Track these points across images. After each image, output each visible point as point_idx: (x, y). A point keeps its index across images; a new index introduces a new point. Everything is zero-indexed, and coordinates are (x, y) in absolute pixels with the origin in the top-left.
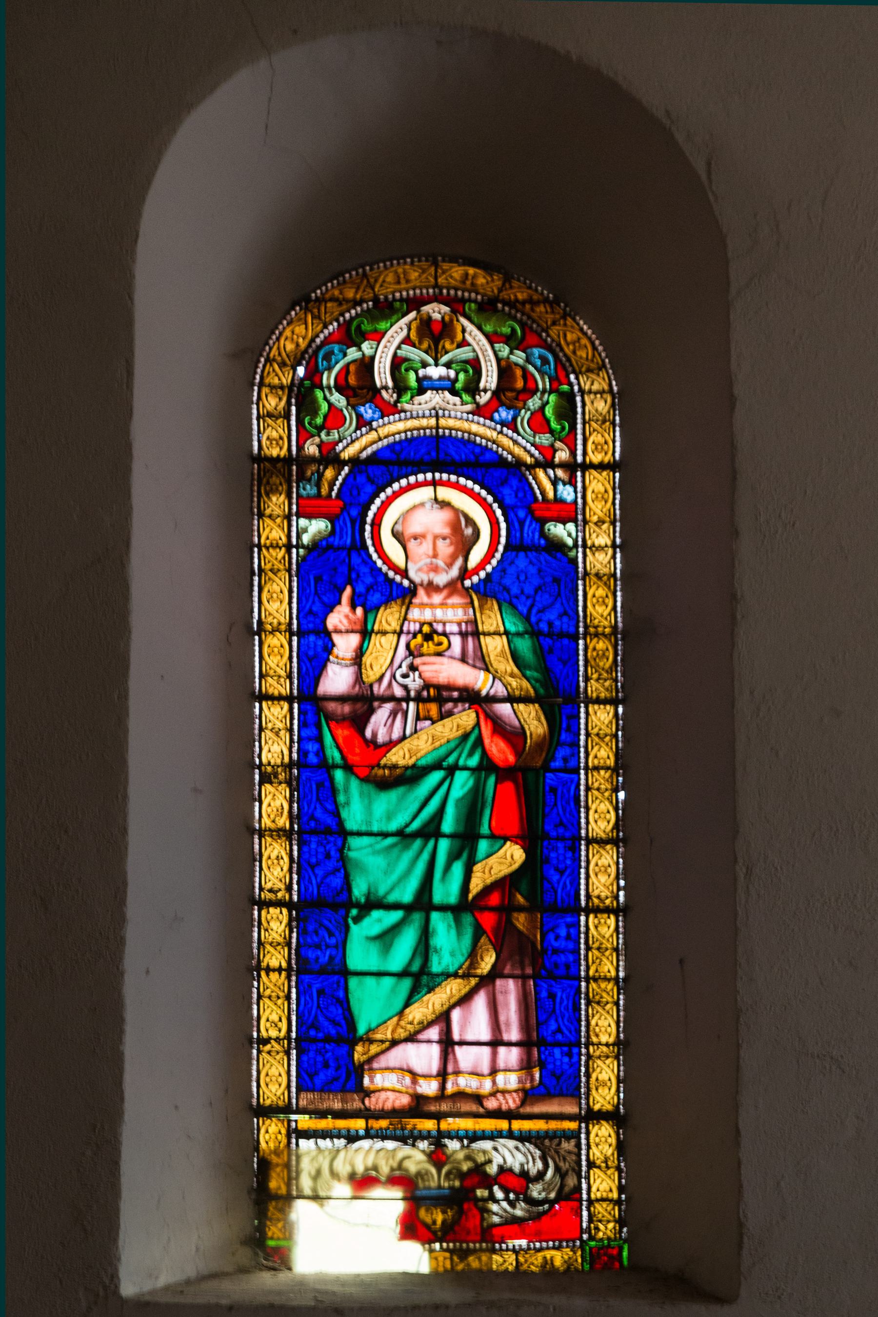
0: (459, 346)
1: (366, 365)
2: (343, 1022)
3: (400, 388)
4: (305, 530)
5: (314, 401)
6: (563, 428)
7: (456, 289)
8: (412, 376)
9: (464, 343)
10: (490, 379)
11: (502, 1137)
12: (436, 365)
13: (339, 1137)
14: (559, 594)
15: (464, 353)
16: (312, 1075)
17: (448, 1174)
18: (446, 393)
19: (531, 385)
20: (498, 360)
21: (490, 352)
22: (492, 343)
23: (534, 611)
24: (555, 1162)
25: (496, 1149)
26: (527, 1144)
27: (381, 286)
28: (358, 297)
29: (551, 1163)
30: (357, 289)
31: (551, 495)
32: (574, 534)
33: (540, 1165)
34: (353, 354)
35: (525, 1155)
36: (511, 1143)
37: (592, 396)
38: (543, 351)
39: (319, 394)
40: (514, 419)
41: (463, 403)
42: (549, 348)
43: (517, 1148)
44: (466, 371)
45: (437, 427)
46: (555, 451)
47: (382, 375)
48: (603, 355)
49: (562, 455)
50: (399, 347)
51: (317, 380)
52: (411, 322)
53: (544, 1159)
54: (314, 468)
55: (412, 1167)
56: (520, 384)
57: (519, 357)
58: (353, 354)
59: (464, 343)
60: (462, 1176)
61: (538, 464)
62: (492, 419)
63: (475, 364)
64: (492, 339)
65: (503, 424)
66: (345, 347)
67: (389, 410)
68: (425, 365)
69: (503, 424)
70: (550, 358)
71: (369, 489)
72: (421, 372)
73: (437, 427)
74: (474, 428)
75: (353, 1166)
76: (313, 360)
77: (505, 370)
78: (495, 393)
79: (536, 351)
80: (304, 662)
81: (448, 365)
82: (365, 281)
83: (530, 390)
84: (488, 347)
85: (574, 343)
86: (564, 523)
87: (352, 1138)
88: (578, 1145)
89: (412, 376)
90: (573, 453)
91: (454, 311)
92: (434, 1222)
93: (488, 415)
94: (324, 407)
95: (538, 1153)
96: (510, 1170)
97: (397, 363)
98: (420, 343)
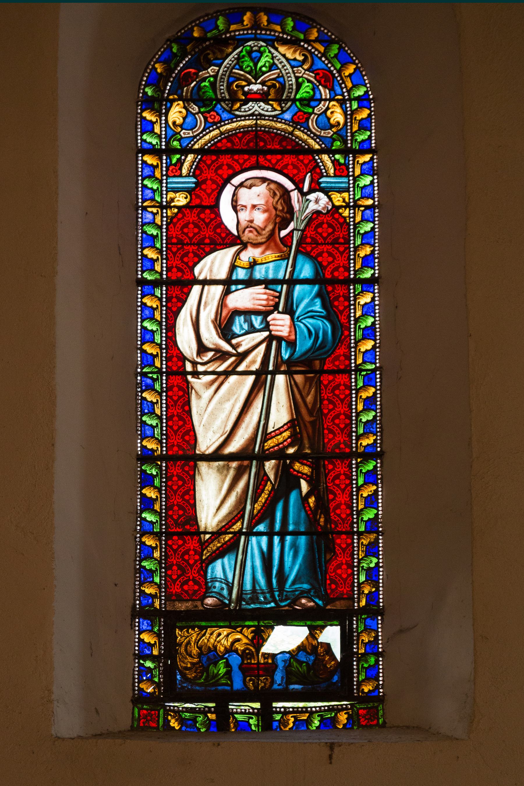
12: (256, 84)
32: (347, 200)
81: (263, 83)
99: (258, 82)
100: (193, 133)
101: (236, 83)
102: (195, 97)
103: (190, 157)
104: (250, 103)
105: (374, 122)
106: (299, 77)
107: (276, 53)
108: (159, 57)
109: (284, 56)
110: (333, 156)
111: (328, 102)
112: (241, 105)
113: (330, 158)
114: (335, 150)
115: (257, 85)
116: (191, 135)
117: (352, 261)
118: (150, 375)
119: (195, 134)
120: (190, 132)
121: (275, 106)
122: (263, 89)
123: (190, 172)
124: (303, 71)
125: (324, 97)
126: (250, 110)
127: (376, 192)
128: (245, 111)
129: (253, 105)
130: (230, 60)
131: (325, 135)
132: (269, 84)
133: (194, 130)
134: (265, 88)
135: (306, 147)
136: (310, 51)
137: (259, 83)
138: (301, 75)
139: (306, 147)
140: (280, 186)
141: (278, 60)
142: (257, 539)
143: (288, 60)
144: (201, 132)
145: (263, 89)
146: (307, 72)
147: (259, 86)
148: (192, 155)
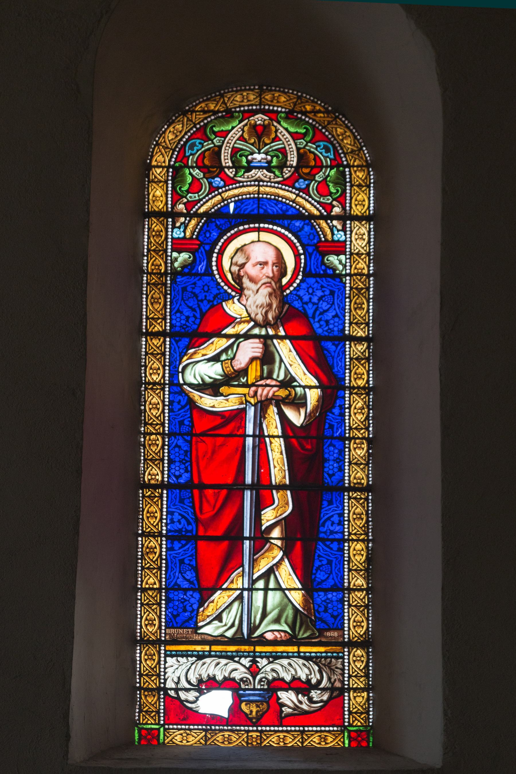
0: (274, 140)
1: (217, 153)
2: (195, 582)
3: (236, 166)
4: (176, 259)
5: (183, 175)
6: (338, 191)
7: (309, 99)
8: (244, 159)
9: (276, 139)
10: (293, 160)
11: (294, 657)
12: (259, 153)
13: (192, 656)
14: (333, 303)
15: (277, 145)
16: (175, 617)
17: (261, 681)
18: (265, 171)
19: (319, 164)
20: (298, 149)
21: (293, 145)
22: (294, 140)
23: (318, 313)
24: (327, 674)
25: (290, 664)
26: (310, 662)
27: (231, 103)
28: (216, 109)
29: (325, 675)
30: (217, 105)
31: (329, 237)
32: (344, 262)
33: (318, 676)
34: (208, 145)
35: (309, 668)
36: (301, 661)
37: (355, 169)
38: (325, 143)
39: (187, 171)
40: (308, 186)
41: (276, 176)
42: (328, 141)
43: (304, 665)
44: (278, 157)
45: (259, 193)
46: (334, 206)
47: (226, 160)
48: (367, 155)
49: (337, 210)
50: (235, 143)
51: (185, 162)
52: (244, 126)
53: (320, 672)
54: (182, 219)
55: (237, 676)
56: (313, 163)
57: (311, 147)
58: (208, 145)
59: (276, 139)
60: (269, 682)
61: (321, 217)
62: (294, 187)
63: (283, 151)
64: (295, 136)
65: (300, 190)
66: (203, 142)
67: (229, 182)
68: (252, 153)
69: (300, 190)
70: (330, 146)
71: (215, 234)
72: (250, 157)
73: (259, 193)
74: (281, 192)
75: (200, 675)
76: (182, 151)
77: (302, 156)
78: (297, 168)
79: (322, 144)
80: (173, 345)
81: (266, 153)
82: (222, 100)
83: (319, 167)
84: (292, 142)
85: (342, 135)
86: (338, 255)
87: (200, 657)
88: (343, 663)
89: (244, 159)
90: (344, 208)
91: (271, 119)
92: (251, 712)
93: (290, 184)
94: (189, 179)
95: (316, 668)
96: (299, 679)
97: (235, 151)
98: (250, 139)
99: (262, 151)
100: (199, 196)
101: (239, 153)
102: (200, 164)
103: (193, 222)
104: (254, 171)
105: (373, 175)
106: (300, 148)
107: (279, 126)
108: (197, 100)
109: (286, 129)
110: (331, 222)
111: (329, 169)
112: (244, 173)
113: (328, 224)
114: (333, 216)
115: (261, 155)
116: (197, 198)
117: (347, 300)
118: (271, 150)
119: (201, 197)
120: (196, 195)
121: (277, 173)
122: (266, 159)
123: (193, 234)
124: (305, 143)
125: (325, 164)
126: (253, 177)
127: (371, 286)
128: (248, 178)
129: (256, 173)
130: (234, 133)
131: (324, 201)
132: (272, 154)
133: (200, 194)
134: (269, 158)
135: (307, 214)
136: (311, 124)
137: (263, 153)
138: (302, 146)
139: (307, 214)
140: (278, 251)
141: (280, 133)
142: (270, 440)
143: (289, 133)
144: (207, 195)
145: (266, 159)
146: (309, 144)
147: (263, 156)
148: (196, 219)
